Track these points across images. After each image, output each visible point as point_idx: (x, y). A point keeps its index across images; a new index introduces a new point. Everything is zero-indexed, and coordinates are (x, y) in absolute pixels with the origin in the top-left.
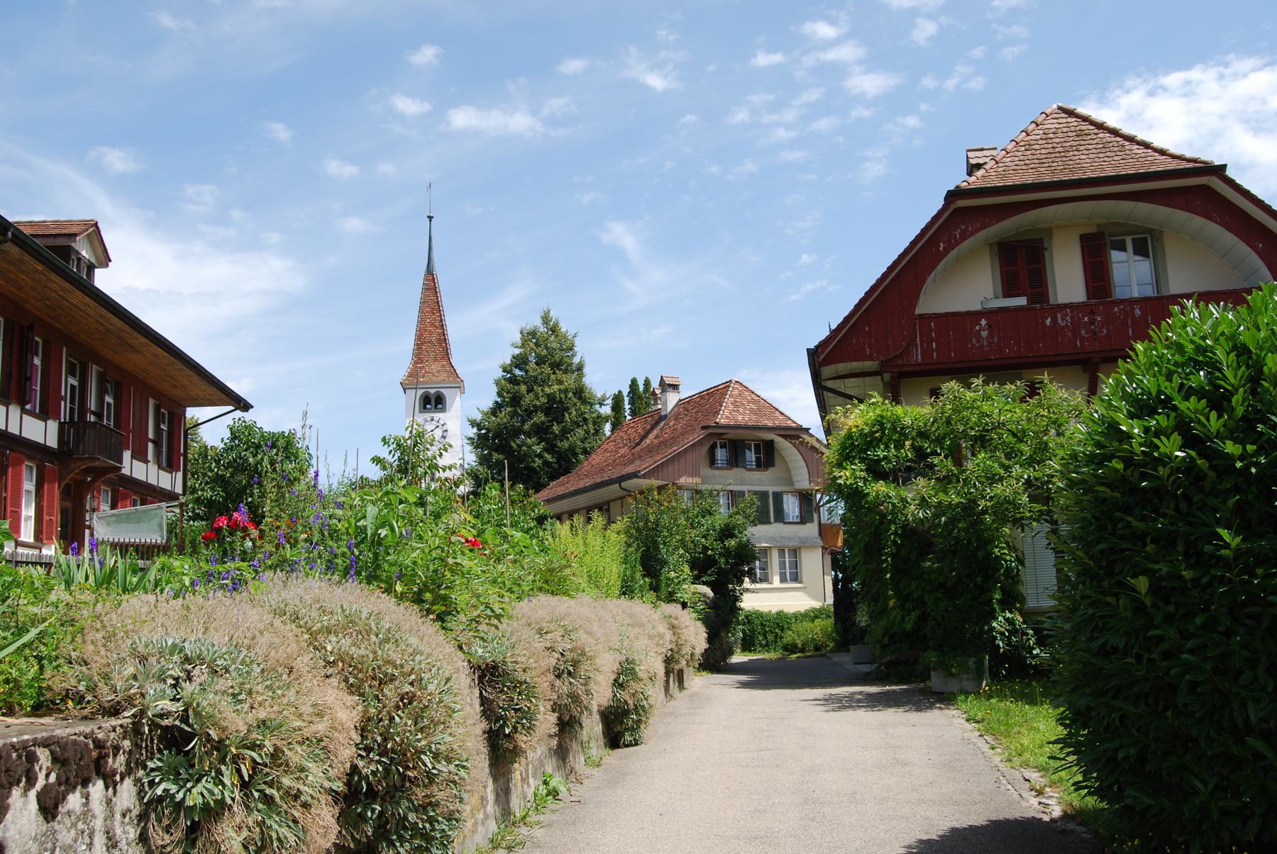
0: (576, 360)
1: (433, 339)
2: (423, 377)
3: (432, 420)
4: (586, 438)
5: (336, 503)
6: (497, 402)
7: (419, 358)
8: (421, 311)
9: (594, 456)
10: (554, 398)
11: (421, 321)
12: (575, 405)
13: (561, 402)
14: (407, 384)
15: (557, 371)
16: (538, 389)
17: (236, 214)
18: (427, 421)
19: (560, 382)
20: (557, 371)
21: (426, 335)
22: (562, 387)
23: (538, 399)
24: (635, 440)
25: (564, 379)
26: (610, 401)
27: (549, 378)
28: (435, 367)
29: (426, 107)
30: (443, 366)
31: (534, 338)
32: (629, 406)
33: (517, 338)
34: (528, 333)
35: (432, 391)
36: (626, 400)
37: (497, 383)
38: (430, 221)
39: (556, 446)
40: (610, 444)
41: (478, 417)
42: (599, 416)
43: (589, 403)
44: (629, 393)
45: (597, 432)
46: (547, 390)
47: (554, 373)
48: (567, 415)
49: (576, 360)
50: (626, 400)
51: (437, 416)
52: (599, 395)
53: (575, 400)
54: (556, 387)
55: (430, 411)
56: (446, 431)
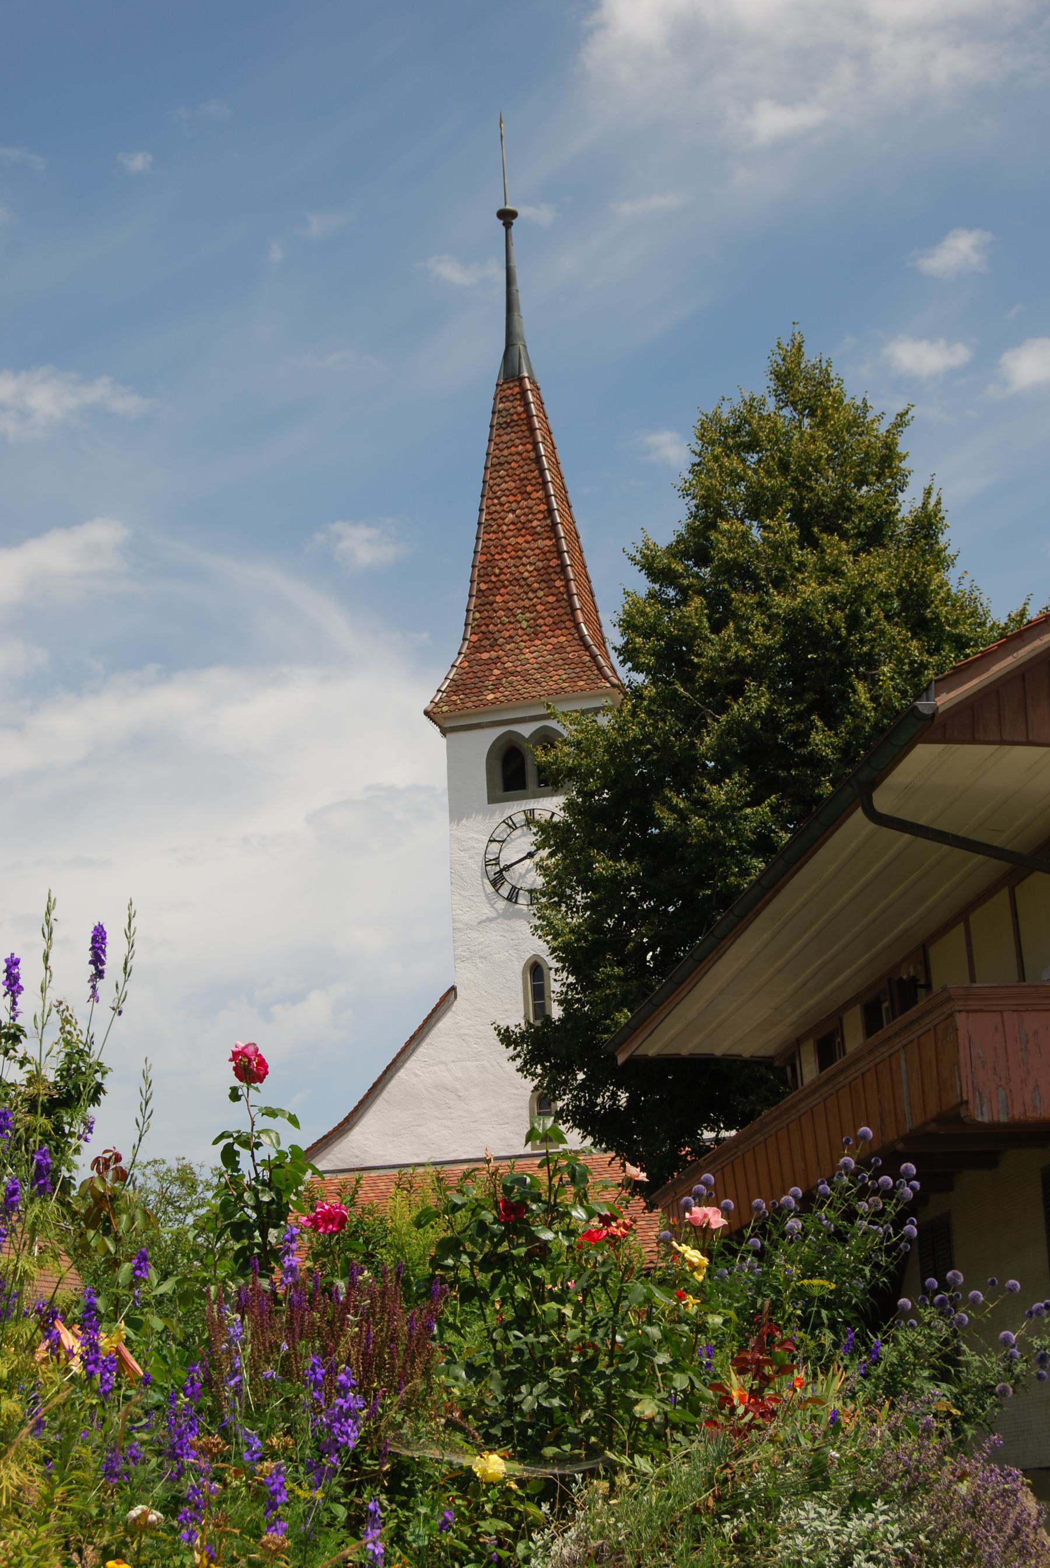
5: (969, 1474)
8: (489, 491)
16: (743, 600)
18: (513, 827)
29: (960, 354)
30: (559, 649)
38: (508, 225)
46: (781, 603)
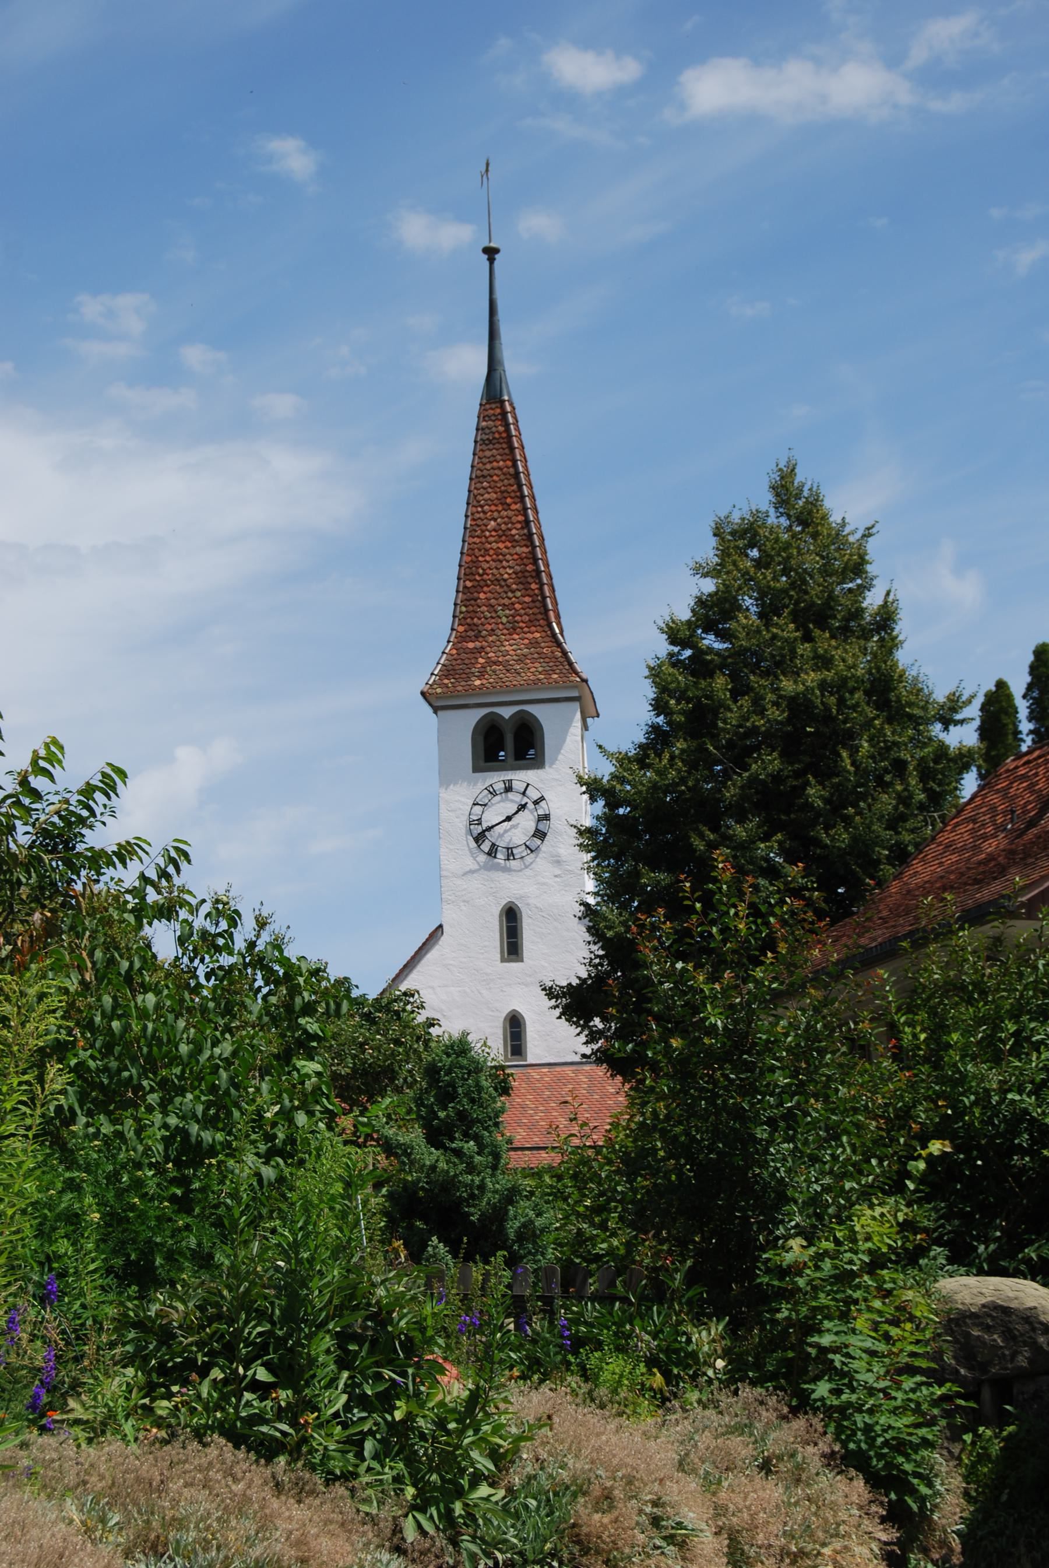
0: (873, 600)
1: (507, 573)
2: (481, 675)
3: (508, 789)
4: (903, 818)
6: (655, 728)
7: (471, 627)
8: (473, 500)
9: (917, 865)
10: (808, 704)
11: (474, 529)
12: (869, 724)
13: (827, 718)
14: (438, 697)
15: (817, 632)
17: (194, 356)
18: (494, 793)
19: (824, 662)
20: (817, 632)
21: (487, 563)
22: (829, 675)
23: (761, 712)
24: (1025, 812)
25: (837, 654)
26: (973, 711)
27: (793, 652)
28: (512, 647)
30: (534, 644)
31: (752, 546)
32: (1031, 726)
33: (707, 550)
34: (733, 533)
35: (507, 712)
36: (1023, 708)
37: (655, 674)
38: (491, 261)
39: (817, 842)
40: (962, 829)
41: (605, 770)
42: (942, 750)
43: (910, 717)
44: (1030, 687)
45: (936, 799)
46: (788, 685)
47: (808, 638)
48: (845, 754)
49: (873, 600)
50: (1023, 708)
51: (520, 777)
52: (940, 696)
53: (870, 712)
54: (811, 678)
55: (504, 767)
56: (546, 817)
